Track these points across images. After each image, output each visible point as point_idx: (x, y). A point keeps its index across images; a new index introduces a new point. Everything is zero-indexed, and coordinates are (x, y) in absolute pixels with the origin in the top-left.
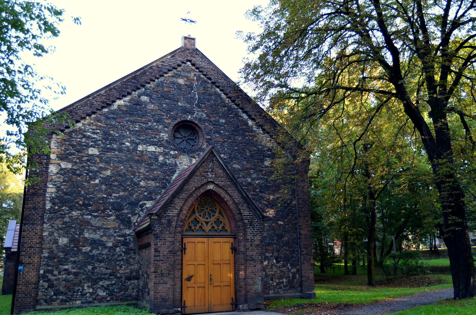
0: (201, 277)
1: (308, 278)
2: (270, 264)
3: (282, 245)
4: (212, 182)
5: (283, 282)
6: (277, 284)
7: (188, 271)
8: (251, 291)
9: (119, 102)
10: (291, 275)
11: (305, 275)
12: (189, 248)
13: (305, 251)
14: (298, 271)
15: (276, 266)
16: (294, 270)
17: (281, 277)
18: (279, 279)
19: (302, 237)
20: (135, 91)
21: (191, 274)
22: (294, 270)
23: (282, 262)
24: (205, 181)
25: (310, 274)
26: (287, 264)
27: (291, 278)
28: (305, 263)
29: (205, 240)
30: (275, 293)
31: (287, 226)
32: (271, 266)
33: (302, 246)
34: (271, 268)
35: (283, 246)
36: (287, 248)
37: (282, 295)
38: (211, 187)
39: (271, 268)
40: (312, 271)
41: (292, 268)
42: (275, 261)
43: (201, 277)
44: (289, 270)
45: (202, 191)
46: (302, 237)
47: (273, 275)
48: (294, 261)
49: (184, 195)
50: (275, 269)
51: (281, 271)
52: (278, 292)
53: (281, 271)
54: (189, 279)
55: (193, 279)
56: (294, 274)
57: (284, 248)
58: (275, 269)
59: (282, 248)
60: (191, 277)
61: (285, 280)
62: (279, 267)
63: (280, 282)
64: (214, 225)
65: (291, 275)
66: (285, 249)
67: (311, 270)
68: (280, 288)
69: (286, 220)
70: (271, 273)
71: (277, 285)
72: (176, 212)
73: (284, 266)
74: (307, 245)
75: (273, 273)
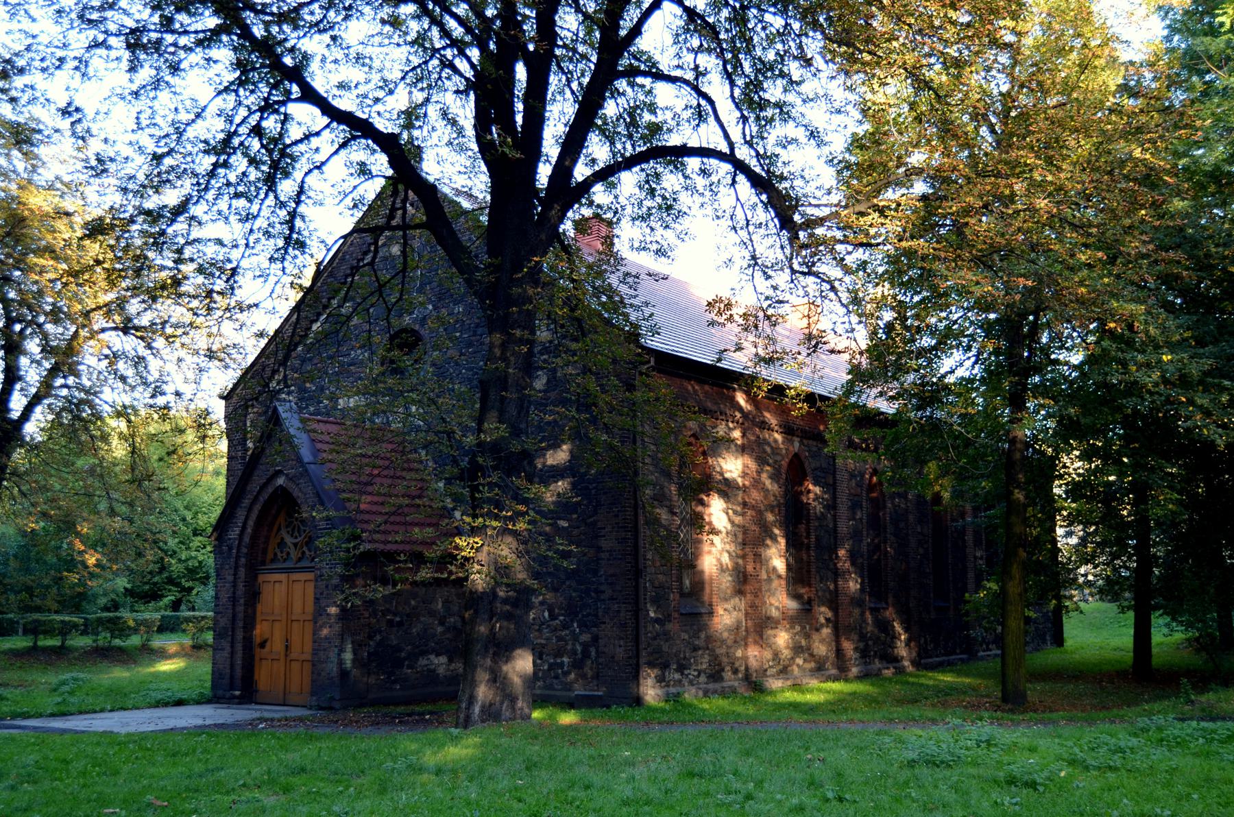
0: (277, 645)
2: (538, 622)
3: (563, 577)
5: (562, 663)
6: (551, 667)
7: (260, 631)
9: (315, 327)
12: (266, 590)
15: (549, 626)
21: (266, 636)
29: (283, 577)
30: (547, 687)
35: (568, 579)
38: (281, 481)
42: (546, 614)
43: (277, 645)
45: (270, 490)
49: (246, 502)
51: (560, 639)
53: (560, 639)
54: (263, 645)
55: (268, 644)
60: (265, 641)
61: (566, 660)
62: (556, 630)
64: (305, 549)
68: (557, 677)
70: (539, 641)
72: (237, 531)
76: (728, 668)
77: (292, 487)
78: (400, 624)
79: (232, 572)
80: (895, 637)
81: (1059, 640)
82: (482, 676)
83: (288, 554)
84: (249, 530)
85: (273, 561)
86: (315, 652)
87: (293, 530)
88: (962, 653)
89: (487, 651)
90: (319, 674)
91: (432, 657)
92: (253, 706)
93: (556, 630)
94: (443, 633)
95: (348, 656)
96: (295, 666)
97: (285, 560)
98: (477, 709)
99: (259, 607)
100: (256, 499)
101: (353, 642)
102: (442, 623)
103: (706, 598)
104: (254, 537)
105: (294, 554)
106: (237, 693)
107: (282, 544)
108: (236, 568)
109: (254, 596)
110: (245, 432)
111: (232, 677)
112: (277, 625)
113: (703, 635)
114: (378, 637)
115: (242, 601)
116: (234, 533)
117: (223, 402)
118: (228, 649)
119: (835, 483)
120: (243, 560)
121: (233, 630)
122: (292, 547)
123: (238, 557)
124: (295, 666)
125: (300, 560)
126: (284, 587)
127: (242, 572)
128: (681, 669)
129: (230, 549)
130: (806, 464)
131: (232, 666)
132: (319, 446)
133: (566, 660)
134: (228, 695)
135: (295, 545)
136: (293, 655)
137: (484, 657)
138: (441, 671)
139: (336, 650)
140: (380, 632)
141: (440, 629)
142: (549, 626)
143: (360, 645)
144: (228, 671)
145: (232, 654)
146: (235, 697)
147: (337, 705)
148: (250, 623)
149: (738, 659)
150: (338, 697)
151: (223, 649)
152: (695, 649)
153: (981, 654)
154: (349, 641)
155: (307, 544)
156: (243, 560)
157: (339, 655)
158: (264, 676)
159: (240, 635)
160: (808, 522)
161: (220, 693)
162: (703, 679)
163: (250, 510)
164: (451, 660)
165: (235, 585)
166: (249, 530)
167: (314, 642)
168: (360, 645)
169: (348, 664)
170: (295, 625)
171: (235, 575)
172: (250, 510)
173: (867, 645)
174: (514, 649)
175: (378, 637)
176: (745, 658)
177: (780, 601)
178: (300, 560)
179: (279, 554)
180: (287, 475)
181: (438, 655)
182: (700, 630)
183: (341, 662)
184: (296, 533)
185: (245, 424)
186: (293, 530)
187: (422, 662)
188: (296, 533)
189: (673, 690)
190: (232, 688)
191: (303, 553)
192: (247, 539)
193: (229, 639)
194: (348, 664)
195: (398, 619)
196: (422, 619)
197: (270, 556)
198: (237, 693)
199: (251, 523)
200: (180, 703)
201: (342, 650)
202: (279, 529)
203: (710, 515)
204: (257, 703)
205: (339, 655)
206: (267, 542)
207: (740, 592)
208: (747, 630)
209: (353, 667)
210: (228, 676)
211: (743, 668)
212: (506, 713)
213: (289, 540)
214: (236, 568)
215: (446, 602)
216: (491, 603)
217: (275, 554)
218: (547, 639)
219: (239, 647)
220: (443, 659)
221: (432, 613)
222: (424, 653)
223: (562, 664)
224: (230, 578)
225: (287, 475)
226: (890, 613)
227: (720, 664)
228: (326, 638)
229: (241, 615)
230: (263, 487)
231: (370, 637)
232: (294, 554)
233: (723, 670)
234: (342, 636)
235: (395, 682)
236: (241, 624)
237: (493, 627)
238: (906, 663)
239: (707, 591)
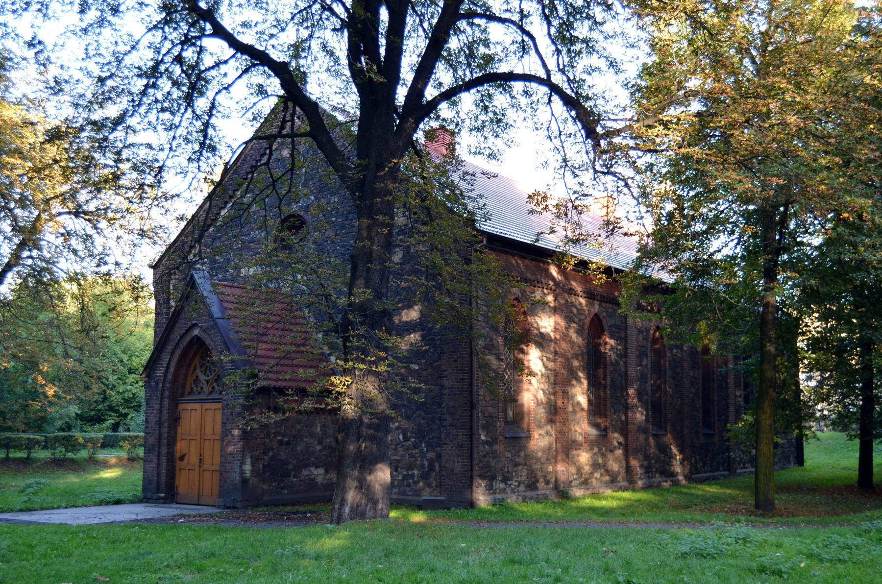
0: (193, 458)
1: (452, 470)
3: (414, 408)
4: (196, 325)
5: (413, 474)
7: (180, 446)
8: (228, 481)
9: (223, 213)
10: (426, 463)
11: (447, 465)
12: (185, 416)
13: (449, 420)
14: (439, 456)
15: (403, 446)
16: (431, 455)
17: (410, 467)
18: (408, 470)
19: (445, 391)
20: (237, 190)
21: (184, 452)
22: (431, 455)
23: (413, 440)
24: (189, 324)
25: (456, 464)
26: (421, 442)
27: (427, 469)
28: (448, 442)
29: (197, 406)
30: (399, 493)
31: (424, 373)
32: (396, 446)
33: (445, 410)
34: (395, 449)
36: (422, 414)
37: (409, 498)
38: (196, 332)
39: (395, 449)
40: (459, 459)
41: (428, 451)
42: (401, 437)
43: (193, 458)
44: (423, 455)
45: (188, 339)
46: (445, 391)
47: (398, 461)
48: (433, 437)
49: (169, 348)
50: (401, 451)
51: (411, 456)
52: (404, 493)
53: (411, 456)
54: (182, 458)
55: (186, 458)
56: (431, 462)
57: (418, 413)
58: (401, 451)
59: (415, 413)
61: (416, 472)
63: (408, 475)
64: (215, 384)
65: (426, 463)
66: (419, 415)
67: (459, 456)
68: (409, 485)
69: (423, 361)
70: (395, 457)
71: (403, 480)
72: (163, 370)
73: (415, 446)
74: (453, 407)
75: (398, 458)
76: (542, 480)
77: (204, 336)
78: (288, 443)
79: (159, 401)
80: (671, 457)
81: (800, 461)
82: (352, 484)
83: (202, 388)
84: (172, 370)
85: (190, 393)
86: (222, 464)
87: (205, 370)
88: (724, 470)
89: (355, 465)
90: (225, 482)
91: (312, 469)
92: (174, 505)
93: (408, 449)
94: (321, 451)
95: (248, 468)
96: (207, 475)
97: (199, 393)
98: (347, 510)
99: (179, 430)
100: (177, 344)
101: (251, 457)
102: (320, 443)
103: (525, 426)
104: (176, 375)
105: (206, 389)
106: (162, 495)
107: (197, 380)
108: (162, 399)
109: (175, 420)
110: (169, 294)
111: (158, 482)
112: (193, 443)
113: (522, 454)
114: (271, 454)
115: (166, 424)
116: (160, 372)
117: (152, 270)
118: (155, 461)
119: (626, 337)
120: (167, 393)
121: (159, 447)
122: (205, 382)
123: (163, 391)
124: (207, 475)
125: (211, 393)
126: (199, 412)
127: (166, 402)
128: (505, 480)
129: (157, 384)
130: (604, 323)
131: (158, 474)
132: (226, 305)
133: (416, 472)
134: (155, 496)
135: (207, 382)
136: (205, 467)
137: (353, 470)
138: (319, 479)
139: (238, 463)
140: (272, 449)
141: (318, 448)
142: (403, 446)
143: (257, 459)
144: (155, 478)
145: (159, 465)
146: (160, 498)
147: (239, 505)
148: (172, 441)
149: (549, 473)
150: (239, 499)
151: (151, 461)
152: (516, 465)
153: (739, 471)
154: (249, 456)
155: (216, 380)
156: (167, 393)
157: (241, 466)
158: (182, 482)
159: (164, 450)
160: (605, 367)
161: (149, 495)
162: (522, 488)
163: (173, 353)
164: (327, 472)
165: (160, 412)
166: (172, 370)
167: (222, 456)
168: (257, 459)
169: (248, 474)
170: (207, 443)
171: (161, 404)
172: (173, 353)
173: (650, 463)
174: (376, 464)
175: (271, 454)
176: (556, 472)
177: (582, 428)
178: (211, 393)
179: (195, 389)
180: (201, 327)
181: (317, 467)
182: (520, 451)
183: (242, 472)
184: (208, 372)
185: (169, 288)
186: (205, 370)
187: (305, 472)
188: (208, 372)
189: (498, 496)
190: (158, 491)
191: (213, 388)
192: (170, 377)
193: (156, 453)
194: (248, 474)
195: (286, 439)
196: (305, 439)
197: (188, 390)
198: (162, 495)
199: (173, 364)
200: (118, 502)
201: (243, 463)
202: (195, 369)
203: (529, 361)
204: (177, 503)
205: (241, 466)
206: (185, 379)
207: (551, 421)
208: (556, 451)
209: (252, 476)
210: (155, 482)
211: (553, 480)
212: (370, 513)
213: (202, 378)
214: (162, 399)
215: (323, 427)
216: (358, 427)
217: (192, 388)
218: (402, 456)
219: (164, 460)
220: (321, 471)
221: (313, 435)
222: (306, 466)
223: (413, 476)
224: (157, 407)
225: (201, 327)
226: (669, 438)
227: (535, 477)
228: (231, 454)
229: (165, 435)
230: (183, 336)
231: (265, 453)
232: (206, 389)
233: (538, 481)
234: (243, 452)
235: (283, 488)
236: (165, 442)
237: (360, 446)
238: (681, 478)
239: (526, 420)
